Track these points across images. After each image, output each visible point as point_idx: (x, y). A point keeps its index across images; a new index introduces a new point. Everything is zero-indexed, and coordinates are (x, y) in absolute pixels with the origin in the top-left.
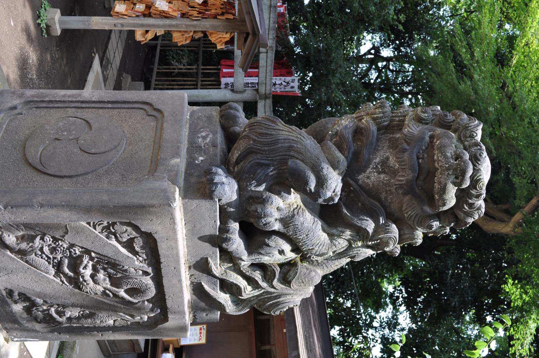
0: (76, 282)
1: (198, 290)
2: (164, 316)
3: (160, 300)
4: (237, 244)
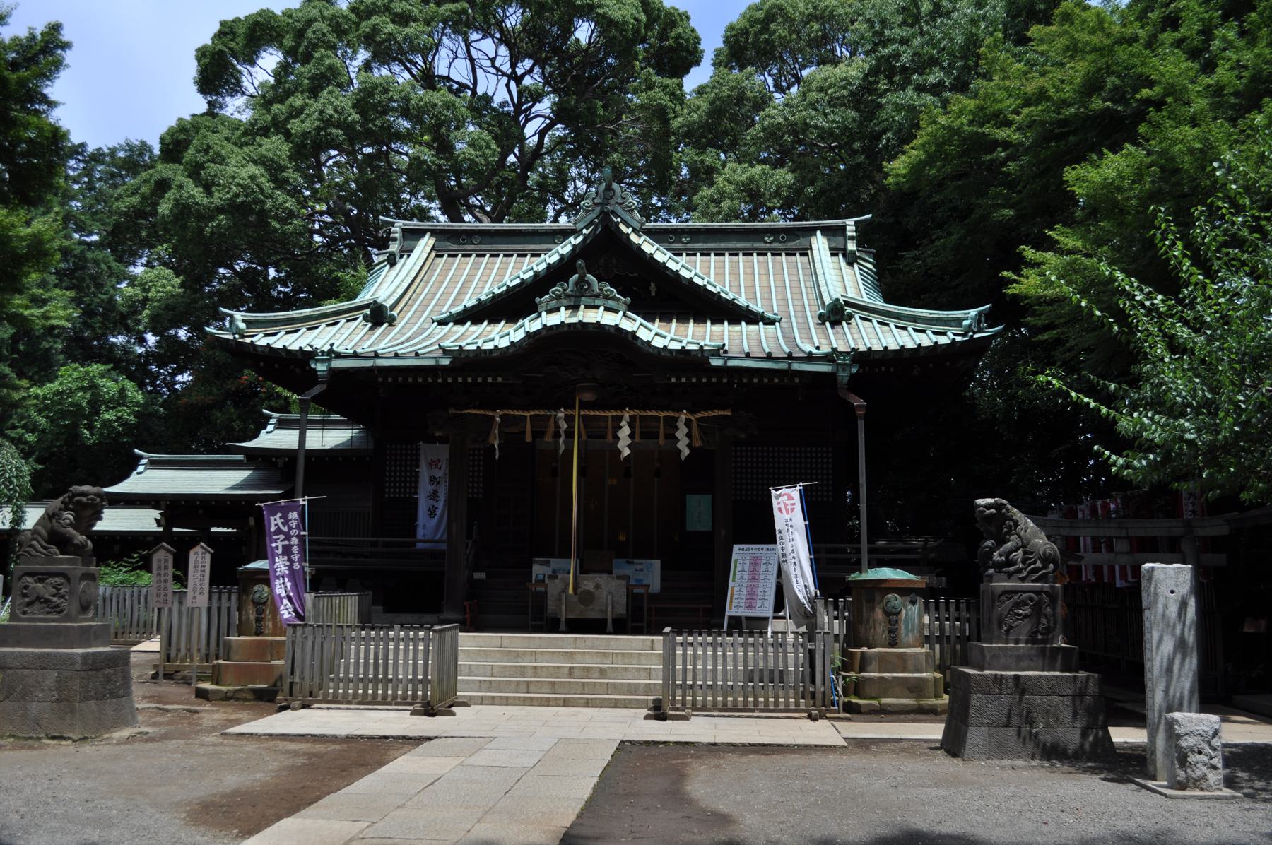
0: (1025, 616)
1: (1033, 581)
2: (1046, 593)
3: (1038, 592)
4: (1012, 569)
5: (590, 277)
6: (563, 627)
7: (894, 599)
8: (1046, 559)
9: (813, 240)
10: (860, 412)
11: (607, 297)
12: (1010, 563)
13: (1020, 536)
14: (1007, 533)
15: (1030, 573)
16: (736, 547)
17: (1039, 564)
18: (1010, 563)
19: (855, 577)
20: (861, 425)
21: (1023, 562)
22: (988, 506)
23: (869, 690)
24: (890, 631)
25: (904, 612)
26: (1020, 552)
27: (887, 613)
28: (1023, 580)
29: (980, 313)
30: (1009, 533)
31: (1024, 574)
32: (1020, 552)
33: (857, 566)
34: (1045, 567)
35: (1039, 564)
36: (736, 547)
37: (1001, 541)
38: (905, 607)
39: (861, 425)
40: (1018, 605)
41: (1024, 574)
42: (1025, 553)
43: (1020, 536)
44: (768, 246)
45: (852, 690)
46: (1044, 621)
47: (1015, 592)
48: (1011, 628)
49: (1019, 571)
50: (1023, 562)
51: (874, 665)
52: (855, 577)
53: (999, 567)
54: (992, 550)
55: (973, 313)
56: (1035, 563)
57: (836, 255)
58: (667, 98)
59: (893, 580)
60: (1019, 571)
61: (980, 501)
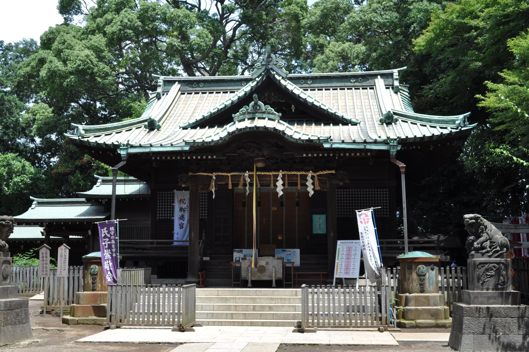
0: (492, 276)
1: (496, 257)
2: (502, 263)
3: (498, 263)
4: (484, 251)
5: (260, 103)
6: (249, 285)
7: (422, 268)
8: (502, 246)
9: (376, 80)
10: (403, 170)
11: (269, 113)
12: (483, 248)
13: (488, 234)
14: (481, 232)
15: (493, 253)
16: (339, 242)
17: (498, 248)
18: (483, 248)
19: (401, 256)
20: (403, 177)
21: (490, 247)
22: (471, 219)
23: (410, 316)
24: (420, 285)
25: (427, 274)
26: (488, 242)
27: (419, 275)
28: (490, 257)
29: (465, 117)
30: (482, 232)
31: (491, 254)
32: (488, 242)
33: (402, 251)
34: (501, 250)
35: (498, 248)
36: (339, 242)
37: (478, 236)
38: (428, 272)
39: (403, 177)
40: (487, 270)
41: (491, 254)
42: (491, 242)
43: (488, 234)
44: (353, 84)
45: (401, 316)
46: (502, 278)
47: (486, 263)
48: (484, 282)
49: (488, 252)
50: (490, 247)
51: (412, 302)
52: (401, 256)
53: (477, 250)
54: (473, 241)
55: (461, 117)
56: (496, 247)
57: (389, 88)
58: (299, 9)
59: (421, 258)
60: (488, 252)
61: (467, 216)
